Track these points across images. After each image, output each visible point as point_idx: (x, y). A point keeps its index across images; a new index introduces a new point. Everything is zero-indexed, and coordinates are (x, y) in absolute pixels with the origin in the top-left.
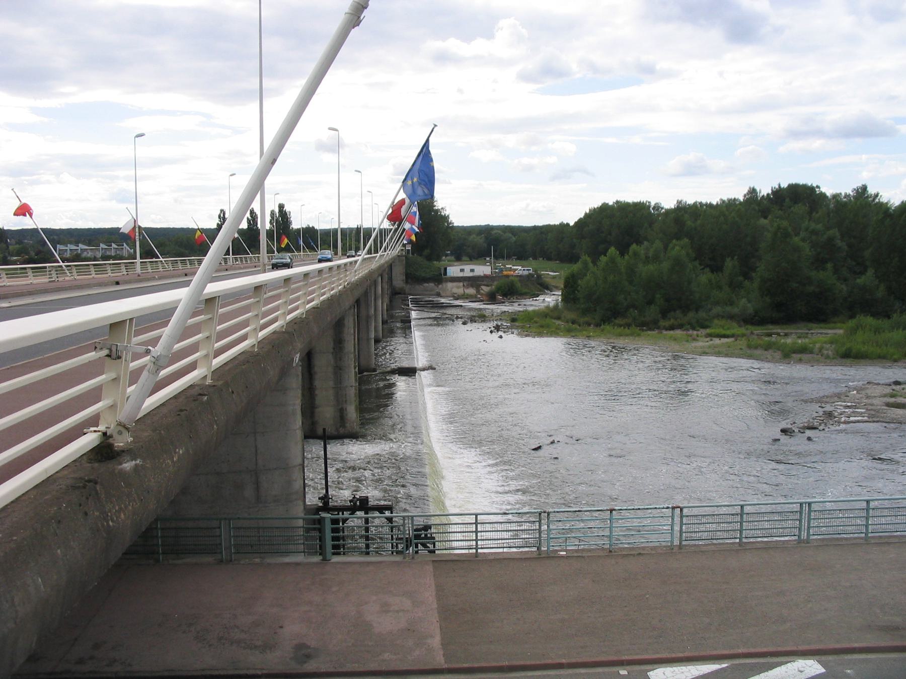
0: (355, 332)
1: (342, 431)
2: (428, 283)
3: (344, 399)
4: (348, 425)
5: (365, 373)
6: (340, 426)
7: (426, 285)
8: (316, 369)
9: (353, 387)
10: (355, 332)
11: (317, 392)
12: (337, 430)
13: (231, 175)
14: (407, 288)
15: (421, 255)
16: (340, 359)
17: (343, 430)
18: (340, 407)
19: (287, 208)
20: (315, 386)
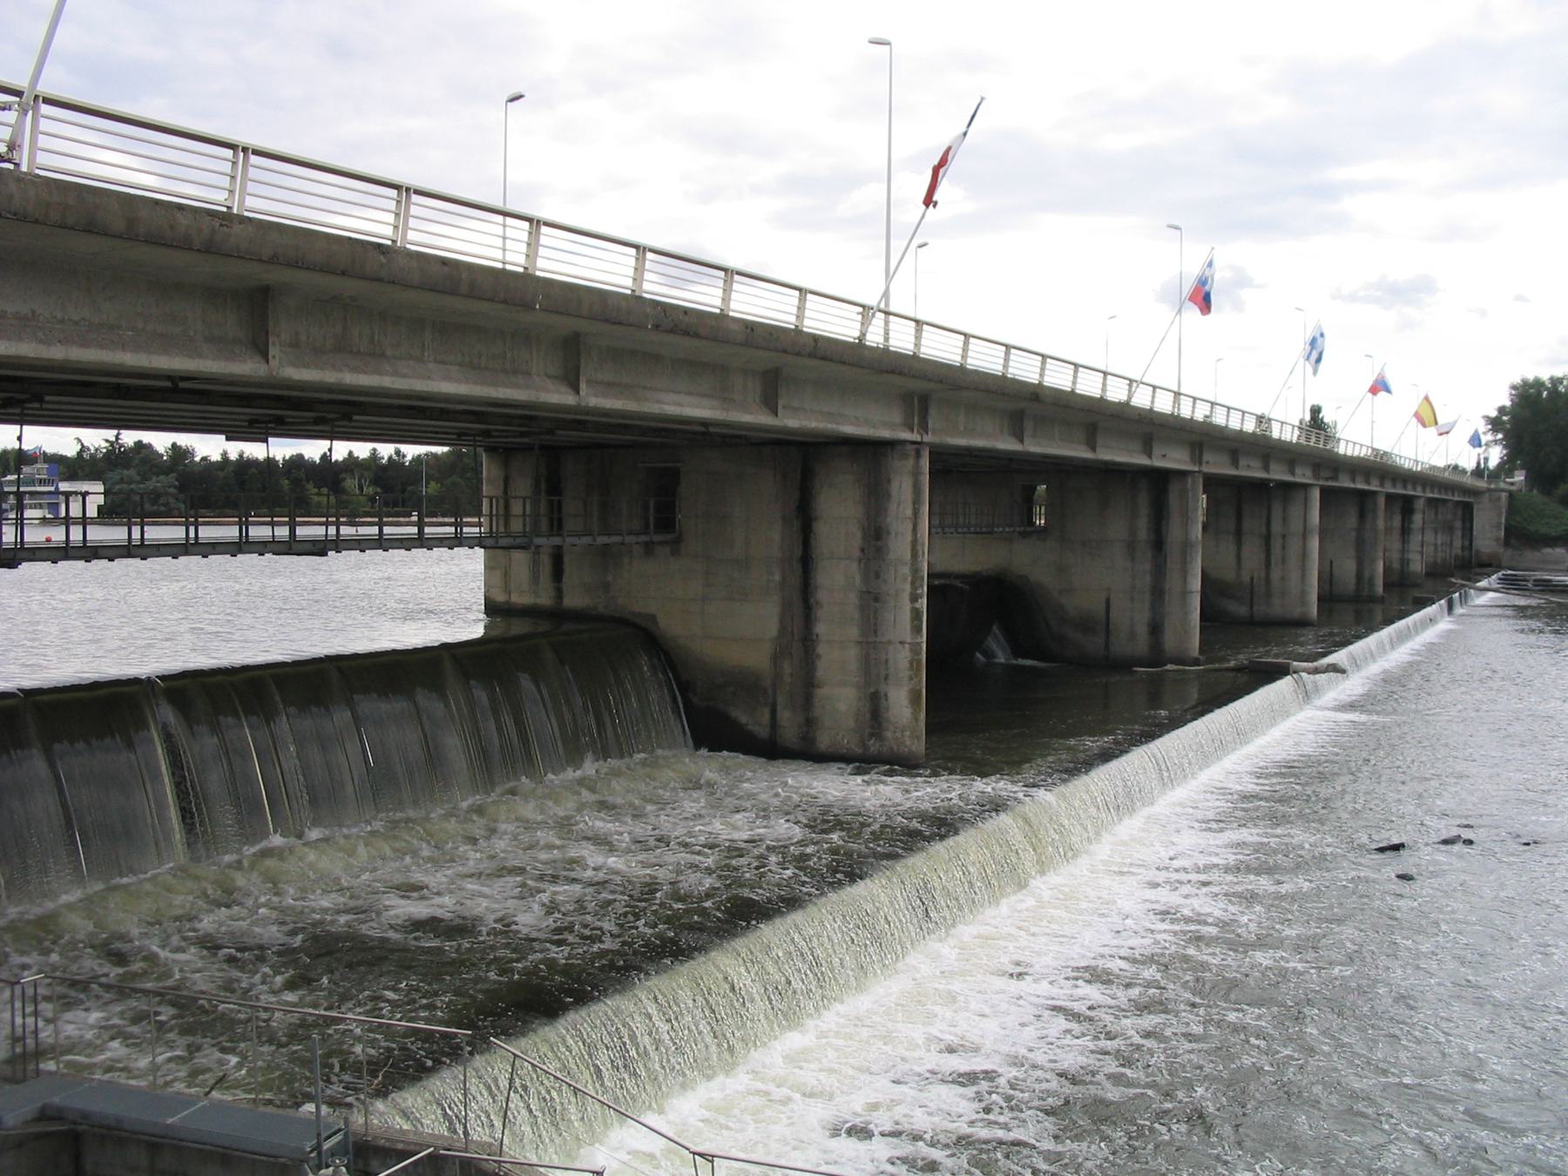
0: (916, 512)
1: (874, 747)
2: (1551, 547)
3: (883, 673)
4: (889, 734)
5: (1169, 667)
6: (872, 735)
7: (1548, 550)
8: (821, 595)
9: (907, 646)
10: (916, 512)
11: (821, 649)
12: (864, 745)
13: (512, 100)
14: (1506, 555)
15: (1548, 493)
16: (877, 576)
17: (877, 744)
18: (872, 690)
19: (1327, 416)
20: (817, 635)
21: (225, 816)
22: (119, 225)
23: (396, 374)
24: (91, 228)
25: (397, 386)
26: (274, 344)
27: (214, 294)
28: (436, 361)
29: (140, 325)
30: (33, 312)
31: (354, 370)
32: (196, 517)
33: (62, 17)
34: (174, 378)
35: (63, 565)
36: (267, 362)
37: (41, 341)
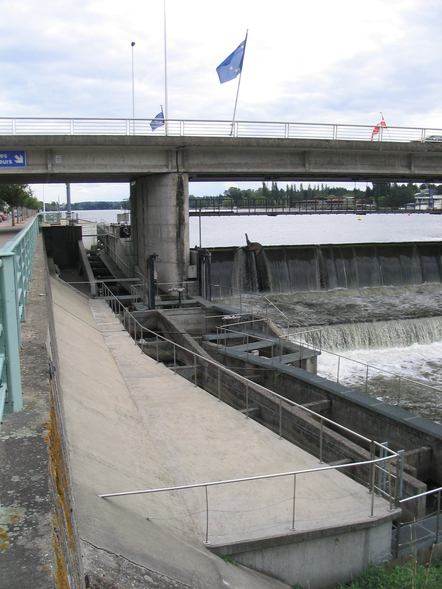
21: (333, 280)
22: (255, 144)
23: (346, 169)
24: (249, 146)
25: (345, 172)
26: (307, 164)
27: (292, 154)
28: (361, 165)
29: (273, 163)
30: (248, 162)
31: (331, 168)
32: (406, 204)
33: (6, 167)
34: (292, 173)
35: (297, 215)
36: (305, 168)
37: (248, 168)
